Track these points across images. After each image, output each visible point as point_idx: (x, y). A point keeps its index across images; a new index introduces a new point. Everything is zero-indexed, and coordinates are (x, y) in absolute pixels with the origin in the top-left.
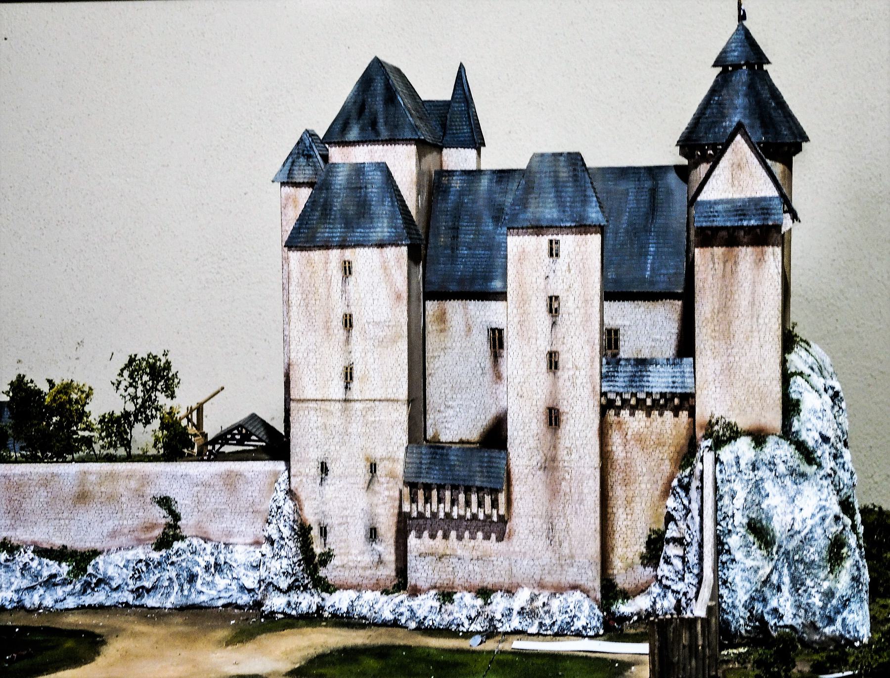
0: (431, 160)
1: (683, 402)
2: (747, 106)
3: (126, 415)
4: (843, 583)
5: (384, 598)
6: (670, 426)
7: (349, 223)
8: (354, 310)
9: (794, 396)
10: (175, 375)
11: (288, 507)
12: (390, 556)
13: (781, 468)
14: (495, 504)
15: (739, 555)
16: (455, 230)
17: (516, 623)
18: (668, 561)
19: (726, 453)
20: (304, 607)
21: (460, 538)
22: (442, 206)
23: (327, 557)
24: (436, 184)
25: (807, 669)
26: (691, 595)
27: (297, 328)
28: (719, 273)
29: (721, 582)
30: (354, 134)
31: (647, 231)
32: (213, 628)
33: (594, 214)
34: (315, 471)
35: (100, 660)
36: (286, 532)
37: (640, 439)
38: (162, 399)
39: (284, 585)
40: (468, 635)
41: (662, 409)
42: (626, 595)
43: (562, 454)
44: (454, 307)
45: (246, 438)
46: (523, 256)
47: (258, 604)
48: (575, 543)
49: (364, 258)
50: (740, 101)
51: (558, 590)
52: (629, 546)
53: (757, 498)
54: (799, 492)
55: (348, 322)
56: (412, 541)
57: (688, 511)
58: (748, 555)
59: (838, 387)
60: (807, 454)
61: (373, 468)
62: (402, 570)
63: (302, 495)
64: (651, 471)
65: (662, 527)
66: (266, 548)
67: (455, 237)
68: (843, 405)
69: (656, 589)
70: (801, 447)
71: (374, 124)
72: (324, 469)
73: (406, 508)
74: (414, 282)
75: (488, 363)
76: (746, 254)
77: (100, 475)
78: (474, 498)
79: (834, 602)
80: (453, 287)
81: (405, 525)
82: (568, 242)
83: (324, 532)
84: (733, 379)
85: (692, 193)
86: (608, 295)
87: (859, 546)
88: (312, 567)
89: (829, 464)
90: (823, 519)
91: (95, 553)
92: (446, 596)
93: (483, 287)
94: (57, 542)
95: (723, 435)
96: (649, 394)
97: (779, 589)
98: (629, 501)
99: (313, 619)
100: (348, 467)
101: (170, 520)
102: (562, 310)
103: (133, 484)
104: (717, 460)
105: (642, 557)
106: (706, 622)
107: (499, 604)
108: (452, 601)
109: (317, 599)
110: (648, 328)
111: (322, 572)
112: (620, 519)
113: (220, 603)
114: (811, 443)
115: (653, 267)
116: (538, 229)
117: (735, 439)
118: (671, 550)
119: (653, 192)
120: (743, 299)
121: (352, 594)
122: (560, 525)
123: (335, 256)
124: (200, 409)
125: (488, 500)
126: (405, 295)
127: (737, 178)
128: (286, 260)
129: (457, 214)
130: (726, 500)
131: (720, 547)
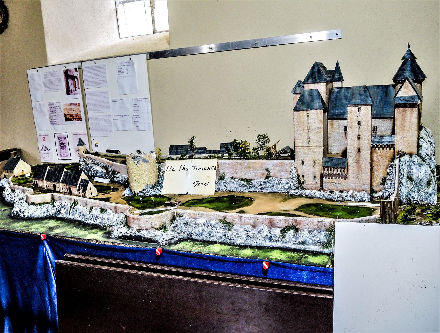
0: (330, 86)
1: (392, 146)
2: (411, 70)
3: (258, 148)
4: (430, 190)
5: (318, 192)
6: (389, 152)
7: (309, 104)
8: (310, 125)
9: (420, 144)
10: (269, 139)
11: (295, 171)
12: (319, 182)
13: (416, 163)
14: (344, 171)
15: (404, 184)
16: (336, 103)
17: (349, 198)
18: (387, 184)
19: (402, 159)
20: (299, 193)
21: (336, 179)
22: (332, 96)
23: (304, 182)
24: (331, 92)
25: (420, 211)
26: (392, 192)
27: (296, 129)
28: (402, 115)
29: (399, 190)
30: (310, 81)
31: (385, 101)
32: (278, 198)
33: (370, 101)
34: (301, 163)
35: (253, 205)
36: (294, 176)
37: (381, 155)
38: (266, 144)
39: (294, 188)
40: (337, 201)
41: (386, 148)
42: (376, 192)
43: (361, 159)
44: (335, 121)
45: (286, 152)
46: (351, 112)
47: (288, 192)
48: (364, 180)
49: (312, 113)
50: (409, 69)
51: (360, 191)
52: (377, 180)
53: (410, 170)
54: (420, 168)
55: (308, 128)
56: (324, 179)
57: (392, 173)
58: (407, 184)
59: (432, 141)
60: (423, 159)
61: (315, 162)
62: (322, 186)
63: (298, 168)
64: (383, 163)
65: (386, 176)
66: (290, 180)
67: (336, 104)
68: (433, 145)
69: (384, 191)
70: (421, 157)
71: (315, 78)
72: (303, 162)
73: (322, 172)
74: (325, 117)
75: (344, 135)
76: (408, 110)
77: (252, 163)
78: (339, 170)
79: (428, 195)
80: (335, 117)
81: (322, 176)
82: (363, 108)
83: (303, 177)
84: (405, 140)
85: (397, 92)
86: (373, 118)
87: (435, 181)
88: (300, 184)
89: (428, 161)
90: (426, 175)
91: (252, 180)
92: (332, 192)
93: (342, 116)
94: (243, 177)
95: (402, 155)
96: (383, 144)
97: (414, 192)
98: (378, 170)
99: (301, 196)
100: (309, 162)
101: (268, 173)
102: (361, 125)
103: (260, 165)
104: (400, 161)
105: (381, 183)
106: (394, 202)
107: (345, 194)
108: (333, 193)
109: (302, 192)
110: (384, 126)
111: (303, 186)
112: (375, 174)
113: (280, 191)
114: (424, 156)
115: (386, 110)
116: (355, 105)
117: (405, 155)
118: (388, 182)
119: (386, 92)
120: (407, 121)
121: (310, 191)
122: (360, 176)
123: (305, 112)
124: (275, 145)
125: (342, 170)
126: (322, 121)
127: (406, 91)
128: (294, 113)
129: (336, 99)
130: (402, 170)
131: (400, 181)
